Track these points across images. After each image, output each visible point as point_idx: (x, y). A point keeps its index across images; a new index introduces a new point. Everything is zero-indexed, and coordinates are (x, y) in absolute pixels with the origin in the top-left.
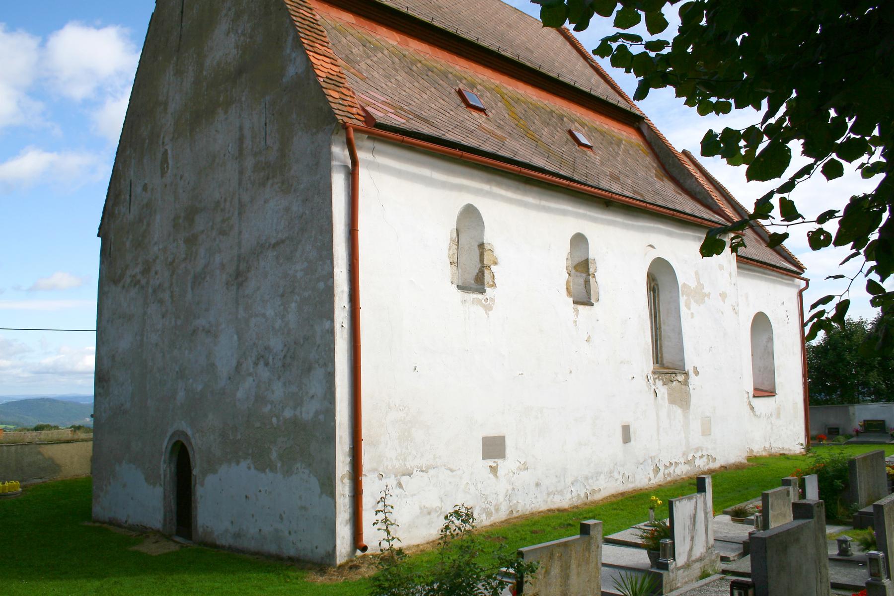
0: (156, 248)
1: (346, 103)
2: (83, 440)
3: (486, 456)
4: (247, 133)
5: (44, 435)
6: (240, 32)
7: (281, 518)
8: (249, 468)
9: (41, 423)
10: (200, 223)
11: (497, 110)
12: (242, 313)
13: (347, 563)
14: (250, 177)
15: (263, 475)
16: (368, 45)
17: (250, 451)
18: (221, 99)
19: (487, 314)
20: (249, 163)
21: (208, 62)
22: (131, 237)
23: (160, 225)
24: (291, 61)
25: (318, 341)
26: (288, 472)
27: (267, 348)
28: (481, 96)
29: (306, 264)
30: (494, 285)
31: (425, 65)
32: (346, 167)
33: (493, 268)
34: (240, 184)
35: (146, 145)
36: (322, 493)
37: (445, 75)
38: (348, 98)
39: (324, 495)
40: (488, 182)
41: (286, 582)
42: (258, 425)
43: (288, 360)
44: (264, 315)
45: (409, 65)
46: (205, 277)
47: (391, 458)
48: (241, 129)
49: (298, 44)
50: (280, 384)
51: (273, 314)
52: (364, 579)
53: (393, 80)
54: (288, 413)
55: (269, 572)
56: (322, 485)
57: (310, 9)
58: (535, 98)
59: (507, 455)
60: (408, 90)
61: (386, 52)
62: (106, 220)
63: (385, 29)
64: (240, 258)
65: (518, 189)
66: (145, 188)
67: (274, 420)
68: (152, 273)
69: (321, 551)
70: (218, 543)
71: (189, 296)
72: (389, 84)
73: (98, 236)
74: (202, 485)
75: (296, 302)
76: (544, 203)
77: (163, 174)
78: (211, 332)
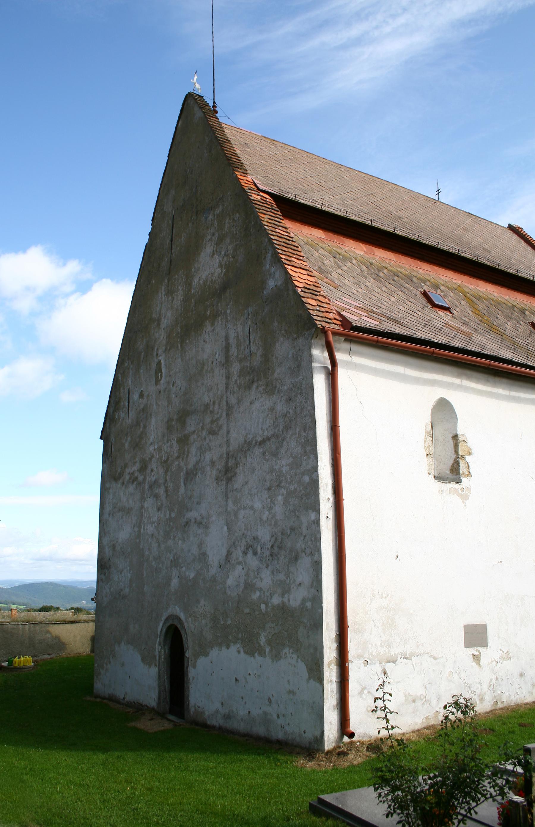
0: (151, 448)
1: (323, 309)
2: (85, 621)
3: (468, 645)
4: (233, 342)
5: (50, 615)
6: (223, 253)
7: (270, 701)
8: (239, 652)
9: (45, 604)
10: (192, 424)
11: (462, 308)
12: (231, 506)
13: (335, 749)
14: (236, 381)
15: (252, 658)
16: (338, 256)
17: (240, 636)
18: (208, 313)
19: (464, 503)
20: (235, 368)
21: (195, 281)
22: (129, 439)
23: (155, 427)
24: (270, 275)
25: (304, 531)
26: (277, 657)
27: (255, 538)
28: (445, 296)
29: (291, 460)
30: (469, 475)
31: (391, 271)
32: (326, 368)
33: (468, 458)
34: (227, 388)
35: (142, 358)
36: (310, 678)
37: (409, 278)
38: (325, 305)
39: (312, 681)
40: (459, 376)
41: (276, 765)
42: (247, 611)
43: (276, 549)
44: (252, 508)
45: (376, 272)
46: (196, 474)
47: (376, 645)
48: (227, 338)
49: (277, 259)
50: (268, 572)
51: (260, 506)
52: (353, 766)
53: (363, 287)
54: (276, 600)
55: (259, 754)
56: (310, 671)
57: (286, 228)
58: (496, 294)
59: (489, 644)
60: (377, 295)
61: (354, 261)
62: (107, 425)
63: (352, 241)
64: (228, 455)
65: (488, 381)
66: (141, 395)
67: (263, 606)
68: (149, 470)
69: (309, 736)
70: (209, 723)
71: (182, 490)
72: (360, 290)
73: (101, 438)
74: (194, 667)
75: (282, 495)
76: (513, 393)
77: (157, 382)
78: (203, 524)
